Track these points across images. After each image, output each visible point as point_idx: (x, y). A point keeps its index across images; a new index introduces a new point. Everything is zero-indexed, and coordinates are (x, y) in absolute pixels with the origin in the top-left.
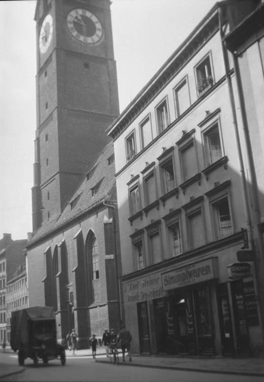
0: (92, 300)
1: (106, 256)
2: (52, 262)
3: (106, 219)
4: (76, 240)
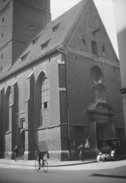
0: (39, 123)
1: (60, 88)
2: (4, 97)
3: (59, 61)
4: (29, 79)
